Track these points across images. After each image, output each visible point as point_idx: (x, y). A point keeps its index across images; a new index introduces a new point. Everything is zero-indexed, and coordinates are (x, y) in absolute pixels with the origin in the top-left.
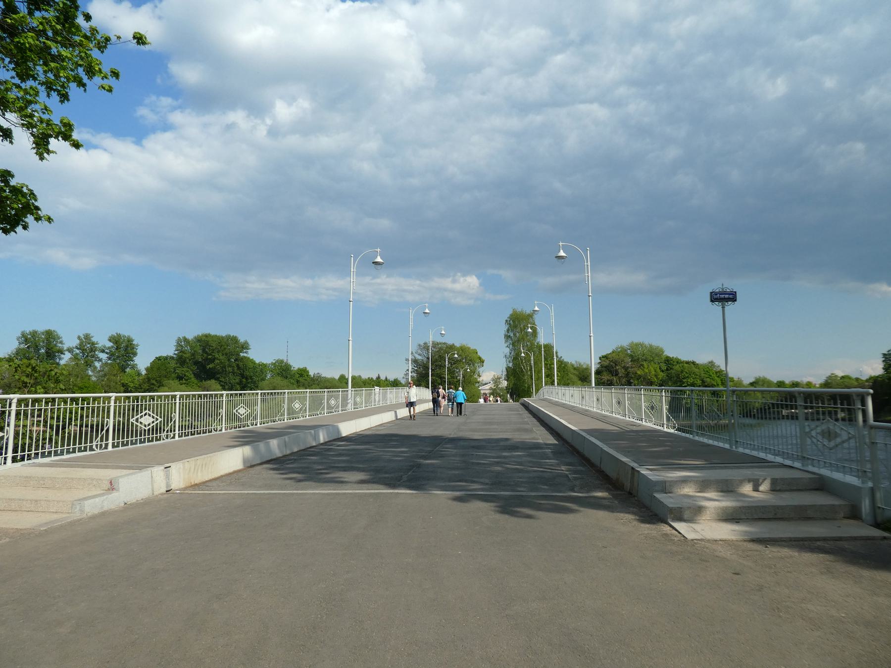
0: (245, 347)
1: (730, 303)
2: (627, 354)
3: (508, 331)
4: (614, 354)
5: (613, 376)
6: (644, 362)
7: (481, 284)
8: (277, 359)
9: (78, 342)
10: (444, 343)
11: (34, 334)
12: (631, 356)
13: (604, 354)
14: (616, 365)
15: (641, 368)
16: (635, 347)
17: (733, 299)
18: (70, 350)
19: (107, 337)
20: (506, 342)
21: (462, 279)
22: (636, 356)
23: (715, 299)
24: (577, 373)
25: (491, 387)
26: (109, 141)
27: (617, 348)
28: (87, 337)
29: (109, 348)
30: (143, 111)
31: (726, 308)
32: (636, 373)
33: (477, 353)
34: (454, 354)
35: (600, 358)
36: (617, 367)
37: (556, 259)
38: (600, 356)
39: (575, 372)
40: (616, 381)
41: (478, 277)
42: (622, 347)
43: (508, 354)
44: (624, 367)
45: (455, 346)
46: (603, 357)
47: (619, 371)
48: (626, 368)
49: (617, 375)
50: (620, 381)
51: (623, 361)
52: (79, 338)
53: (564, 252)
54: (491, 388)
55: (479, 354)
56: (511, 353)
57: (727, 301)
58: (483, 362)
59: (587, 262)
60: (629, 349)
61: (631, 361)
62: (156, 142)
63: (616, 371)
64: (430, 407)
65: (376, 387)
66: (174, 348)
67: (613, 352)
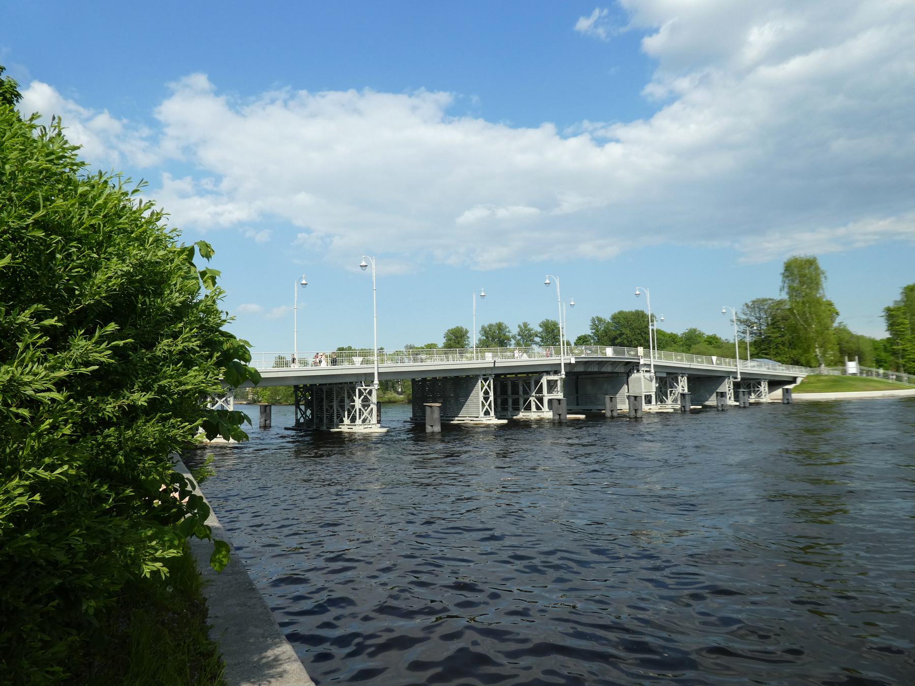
8: (689, 328)
9: (518, 330)
11: (491, 325)
18: (514, 337)
19: (540, 321)
26: (620, 131)
28: (525, 325)
29: (540, 333)
30: (650, 89)
52: (519, 326)
62: (661, 120)
64: (850, 369)
65: (639, 348)
66: (589, 327)
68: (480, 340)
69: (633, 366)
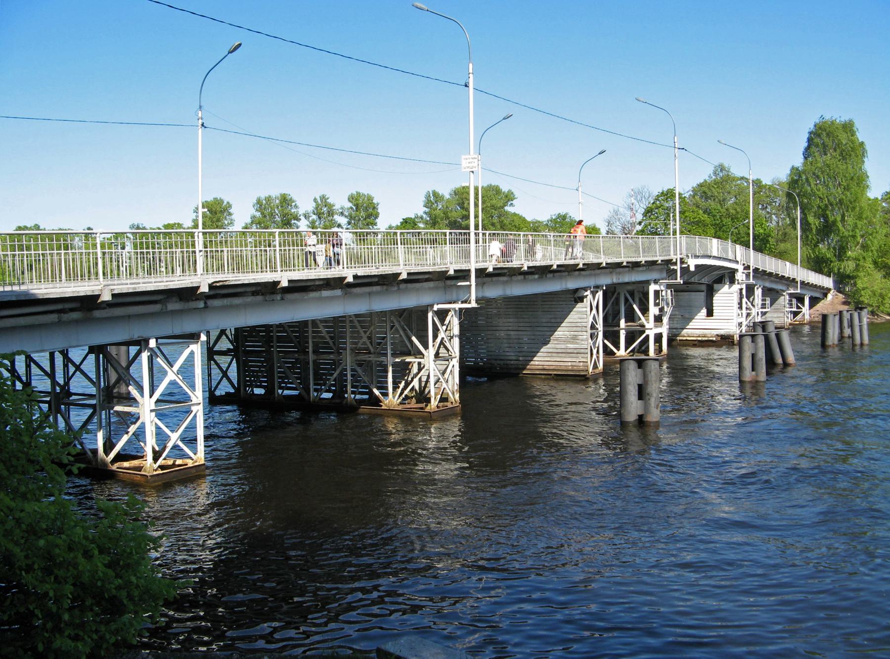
0: (509, 197)
9: (314, 204)
11: (269, 199)
18: (306, 216)
28: (323, 198)
52: (315, 200)
68: (253, 217)
69: (746, 320)
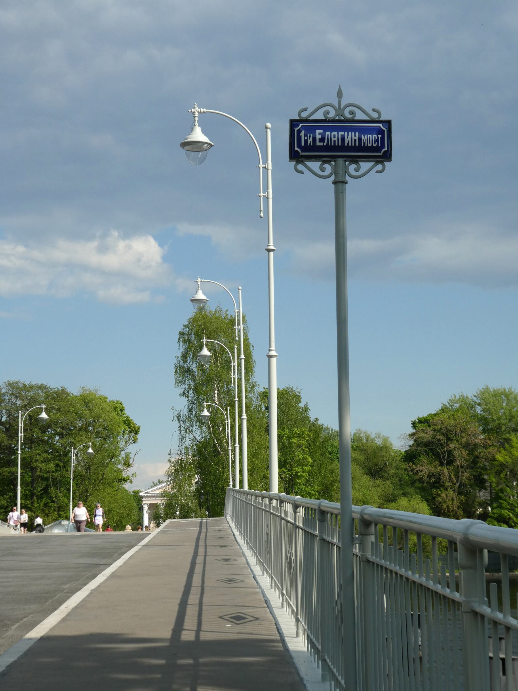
1: (365, 166)
2: (475, 416)
3: (184, 356)
4: (445, 415)
5: (442, 464)
6: (513, 434)
7: (165, 258)
10: (42, 387)
12: (484, 421)
13: (424, 414)
14: (449, 439)
15: (505, 449)
16: (491, 400)
17: (377, 149)
20: (179, 383)
21: (122, 245)
22: (494, 420)
23: (306, 148)
24: (362, 458)
25: (165, 491)
27: (452, 402)
31: (351, 184)
32: (494, 459)
33: (122, 410)
34: (40, 411)
35: (414, 424)
36: (452, 446)
37: (183, 151)
38: (414, 418)
39: (357, 455)
40: (450, 476)
41: (161, 241)
42: (463, 400)
43: (185, 412)
44: (466, 446)
45: (68, 395)
46: (420, 422)
47: (456, 453)
48: (471, 448)
49: (450, 462)
50: (457, 477)
51: (464, 430)
53: (204, 132)
54: (164, 494)
55: (129, 412)
56: (191, 411)
57: (355, 160)
58: (136, 432)
59: (265, 161)
60: (479, 404)
61: (484, 431)
63: (450, 453)
67: (443, 411)
